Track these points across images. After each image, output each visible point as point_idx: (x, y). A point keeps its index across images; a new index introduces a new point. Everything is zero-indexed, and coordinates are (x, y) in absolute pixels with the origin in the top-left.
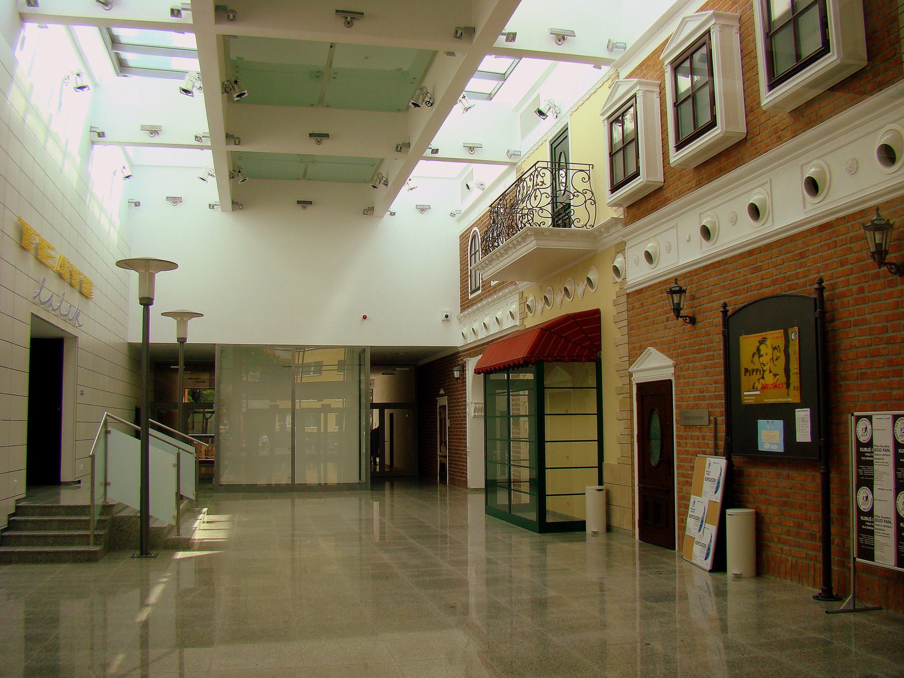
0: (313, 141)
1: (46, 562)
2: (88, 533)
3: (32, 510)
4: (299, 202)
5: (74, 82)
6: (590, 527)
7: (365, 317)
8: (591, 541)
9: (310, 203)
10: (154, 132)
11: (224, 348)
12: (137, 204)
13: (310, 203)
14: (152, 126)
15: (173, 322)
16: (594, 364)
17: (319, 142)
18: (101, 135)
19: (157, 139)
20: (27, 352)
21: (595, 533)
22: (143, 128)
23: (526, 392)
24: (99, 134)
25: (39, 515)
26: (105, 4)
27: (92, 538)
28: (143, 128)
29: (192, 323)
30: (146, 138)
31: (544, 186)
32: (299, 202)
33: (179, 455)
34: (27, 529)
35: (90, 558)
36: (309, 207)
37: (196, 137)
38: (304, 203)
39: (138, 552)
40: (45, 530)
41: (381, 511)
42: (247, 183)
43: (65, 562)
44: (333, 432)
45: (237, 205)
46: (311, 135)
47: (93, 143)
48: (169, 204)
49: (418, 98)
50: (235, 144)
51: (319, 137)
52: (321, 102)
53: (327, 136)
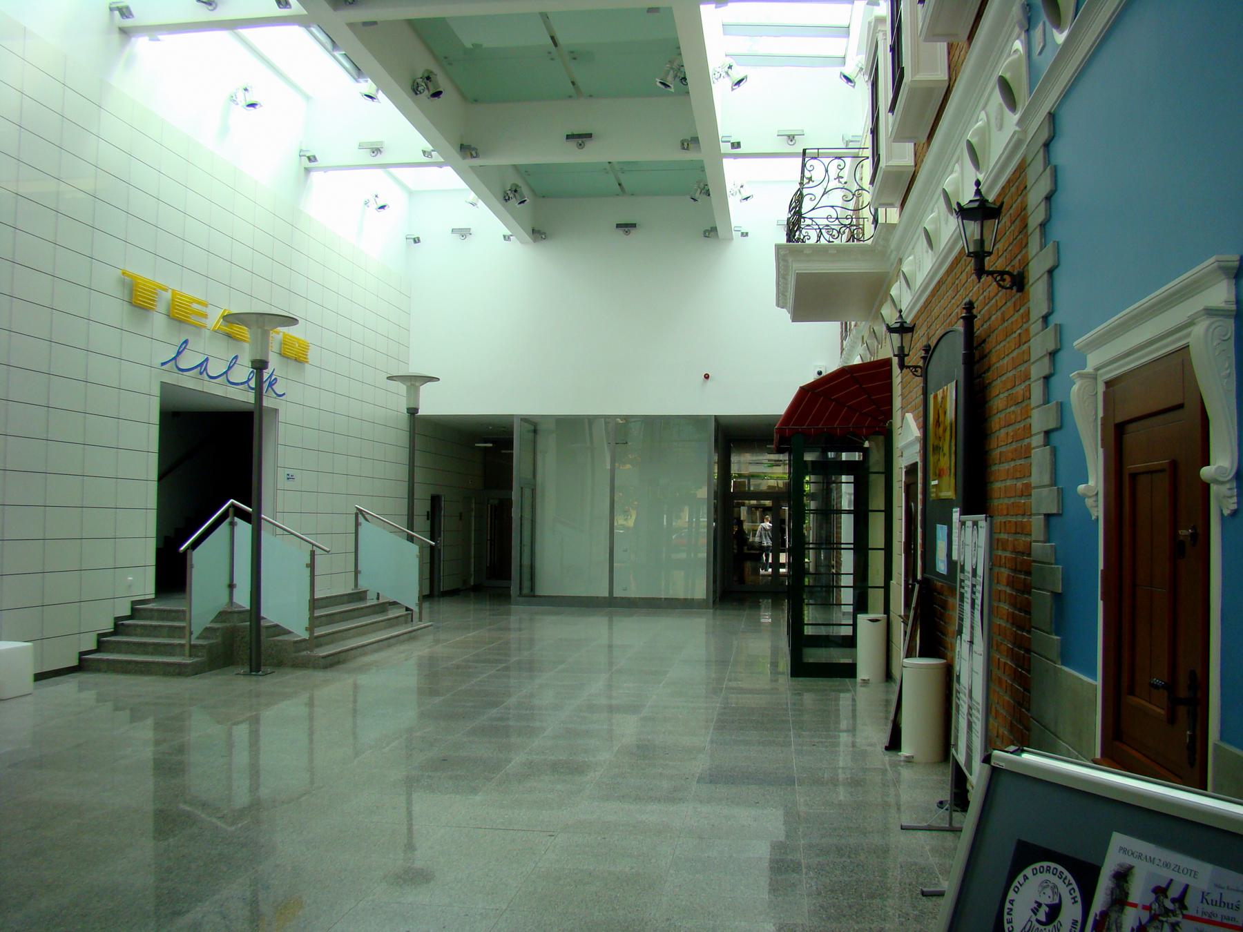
0: (572, 144)
1: (116, 671)
2: (183, 642)
3: (150, 614)
4: (619, 226)
5: (243, 99)
6: (863, 673)
7: (707, 377)
8: (862, 693)
9: (634, 226)
10: (376, 151)
11: (533, 425)
12: (417, 241)
13: (634, 226)
14: (372, 143)
15: (402, 388)
16: (881, 438)
17: (581, 146)
18: (312, 159)
19: (380, 159)
20: (155, 431)
21: (865, 682)
22: (361, 146)
23: (851, 478)
24: (309, 158)
25: (158, 619)
26: (209, 4)
27: (187, 647)
28: (361, 146)
29: (425, 389)
30: (367, 158)
31: (811, 184)
32: (619, 226)
33: (313, 554)
34: (136, 635)
35: (179, 671)
36: (633, 231)
37: (424, 152)
38: (627, 227)
39: (247, 669)
40: (156, 636)
41: (459, 633)
42: (539, 205)
43: (156, 674)
44: (673, 538)
45: (538, 234)
46: (568, 137)
47: (308, 170)
48: (456, 237)
49: (667, 74)
50: (472, 156)
51: (580, 138)
52: (576, 90)
53: (589, 136)
